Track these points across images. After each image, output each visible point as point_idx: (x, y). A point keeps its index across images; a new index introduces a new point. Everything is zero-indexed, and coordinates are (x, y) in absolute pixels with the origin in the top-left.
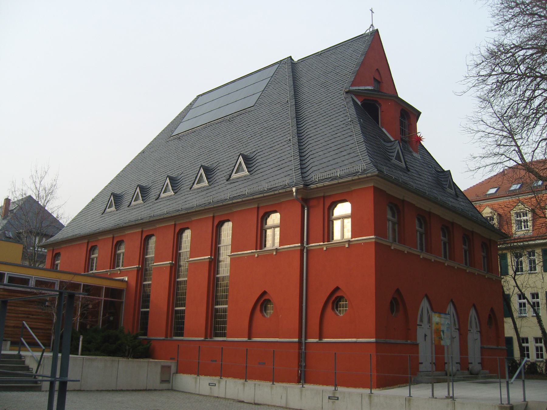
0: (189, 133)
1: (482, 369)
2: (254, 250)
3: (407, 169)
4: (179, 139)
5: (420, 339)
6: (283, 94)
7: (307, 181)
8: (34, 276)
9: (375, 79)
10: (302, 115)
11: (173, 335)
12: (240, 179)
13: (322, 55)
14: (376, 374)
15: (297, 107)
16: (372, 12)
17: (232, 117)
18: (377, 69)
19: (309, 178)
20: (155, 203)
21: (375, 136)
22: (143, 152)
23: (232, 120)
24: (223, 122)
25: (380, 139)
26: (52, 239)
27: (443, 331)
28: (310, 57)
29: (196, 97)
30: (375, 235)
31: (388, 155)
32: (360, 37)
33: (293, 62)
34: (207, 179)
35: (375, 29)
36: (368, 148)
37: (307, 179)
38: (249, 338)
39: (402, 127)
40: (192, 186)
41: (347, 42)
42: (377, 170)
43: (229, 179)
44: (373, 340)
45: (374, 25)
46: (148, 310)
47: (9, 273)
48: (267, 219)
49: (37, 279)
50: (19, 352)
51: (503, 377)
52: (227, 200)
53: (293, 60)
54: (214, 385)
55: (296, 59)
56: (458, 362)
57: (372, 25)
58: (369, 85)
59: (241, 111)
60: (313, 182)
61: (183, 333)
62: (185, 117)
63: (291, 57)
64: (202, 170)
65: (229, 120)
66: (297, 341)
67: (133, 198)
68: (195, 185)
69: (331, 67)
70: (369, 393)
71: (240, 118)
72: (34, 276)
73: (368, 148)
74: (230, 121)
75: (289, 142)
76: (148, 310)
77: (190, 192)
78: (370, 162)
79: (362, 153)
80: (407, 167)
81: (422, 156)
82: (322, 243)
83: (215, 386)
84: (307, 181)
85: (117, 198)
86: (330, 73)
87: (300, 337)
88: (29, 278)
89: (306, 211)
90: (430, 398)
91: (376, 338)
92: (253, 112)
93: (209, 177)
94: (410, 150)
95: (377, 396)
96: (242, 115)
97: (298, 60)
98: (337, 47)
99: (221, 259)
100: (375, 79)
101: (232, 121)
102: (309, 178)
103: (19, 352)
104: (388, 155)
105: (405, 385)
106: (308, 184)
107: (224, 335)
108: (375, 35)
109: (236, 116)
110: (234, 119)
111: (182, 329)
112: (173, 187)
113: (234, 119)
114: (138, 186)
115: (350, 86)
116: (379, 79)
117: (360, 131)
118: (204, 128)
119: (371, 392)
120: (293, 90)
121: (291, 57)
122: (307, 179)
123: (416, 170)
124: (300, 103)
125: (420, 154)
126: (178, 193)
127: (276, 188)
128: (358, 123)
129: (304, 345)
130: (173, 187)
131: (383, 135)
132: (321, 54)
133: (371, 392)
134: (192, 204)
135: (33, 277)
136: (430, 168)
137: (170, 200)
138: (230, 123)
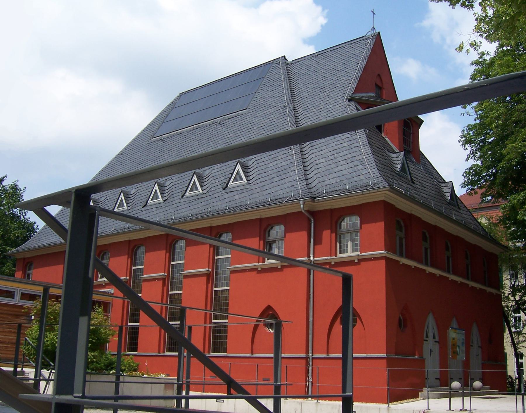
0: (175, 135)
1: (483, 386)
2: (257, 263)
3: (413, 181)
4: (163, 140)
5: (426, 354)
6: (279, 98)
7: (314, 193)
8: (19, 289)
9: (376, 85)
10: (302, 121)
11: (166, 351)
12: (239, 188)
13: (319, 56)
14: (386, 388)
15: (295, 113)
16: (374, 13)
17: (223, 119)
18: (379, 75)
19: (314, 189)
20: (142, 211)
21: (380, 147)
22: (122, 154)
23: (223, 123)
24: (213, 125)
25: (385, 150)
26: (23, 247)
27: (459, 346)
28: (307, 58)
29: (178, 95)
30: (385, 250)
31: (394, 167)
32: (361, 39)
33: (287, 62)
34: (201, 186)
35: (377, 31)
36: (376, 160)
37: (312, 190)
38: (252, 353)
39: (405, 136)
40: (185, 193)
41: (347, 44)
42: (388, 184)
43: (226, 187)
44: (384, 355)
45: (375, 27)
46: (138, 324)
47: (21, 289)
48: (269, 231)
49: (23, 292)
50: (22, 369)
51: (387, 403)
52: (227, 211)
53: (287, 60)
54: (223, 401)
55: (290, 60)
56: (437, 378)
57: (373, 27)
58: (371, 92)
59: (233, 114)
60: (320, 194)
61: (137, 348)
62: (167, 116)
63: (284, 57)
64: (196, 177)
65: (219, 123)
66: (178, 355)
67: (116, 204)
68: (188, 192)
69: (330, 71)
70: (387, 407)
71: (232, 121)
72: (19, 289)
73: (376, 160)
74: (221, 124)
75: (291, 150)
76: (138, 324)
77: (182, 200)
78: (380, 175)
79: (370, 165)
80: (412, 179)
81: (423, 166)
82: (329, 257)
83: (223, 402)
84: (314, 193)
85: (97, 203)
86: (330, 77)
87: (307, 352)
88: (14, 290)
89: (312, 224)
90: (447, 410)
91: (387, 353)
92: (247, 115)
93: (203, 184)
94: (412, 160)
95: (395, 409)
96: (234, 118)
97: (293, 61)
98: (336, 49)
99: (219, 272)
100: (376, 85)
101: (224, 124)
102: (314, 189)
103: (22, 369)
104: (394, 167)
105: (413, 400)
106: (315, 196)
107: (225, 351)
108: (378, 38)
109: (227, 118)
110: (225, 122)
111: (136, 344)
112: (162, 194)
113: (225, 122)
114: (121, 192)
115: (352, 93)
116: (380, 84)
117: (367, 142)
118: (191, 130)
119: (389, 406)
120: (290, 94)
121: (284, 57)
122: (312, 190)
123: (420, 182)
124: (298, 108)
125: (422, 164)
126: (168, 201)
127: (280, 200)
128: (364, 133)
129: (311, 360)
130: (162, 194)
131: (387, 145)
132: (318, 55)
133: (389, 406)
134: (187, 213)
135: (19, 290)
136: (432, 178)
137: (159, 208)
138: (221, 126)
